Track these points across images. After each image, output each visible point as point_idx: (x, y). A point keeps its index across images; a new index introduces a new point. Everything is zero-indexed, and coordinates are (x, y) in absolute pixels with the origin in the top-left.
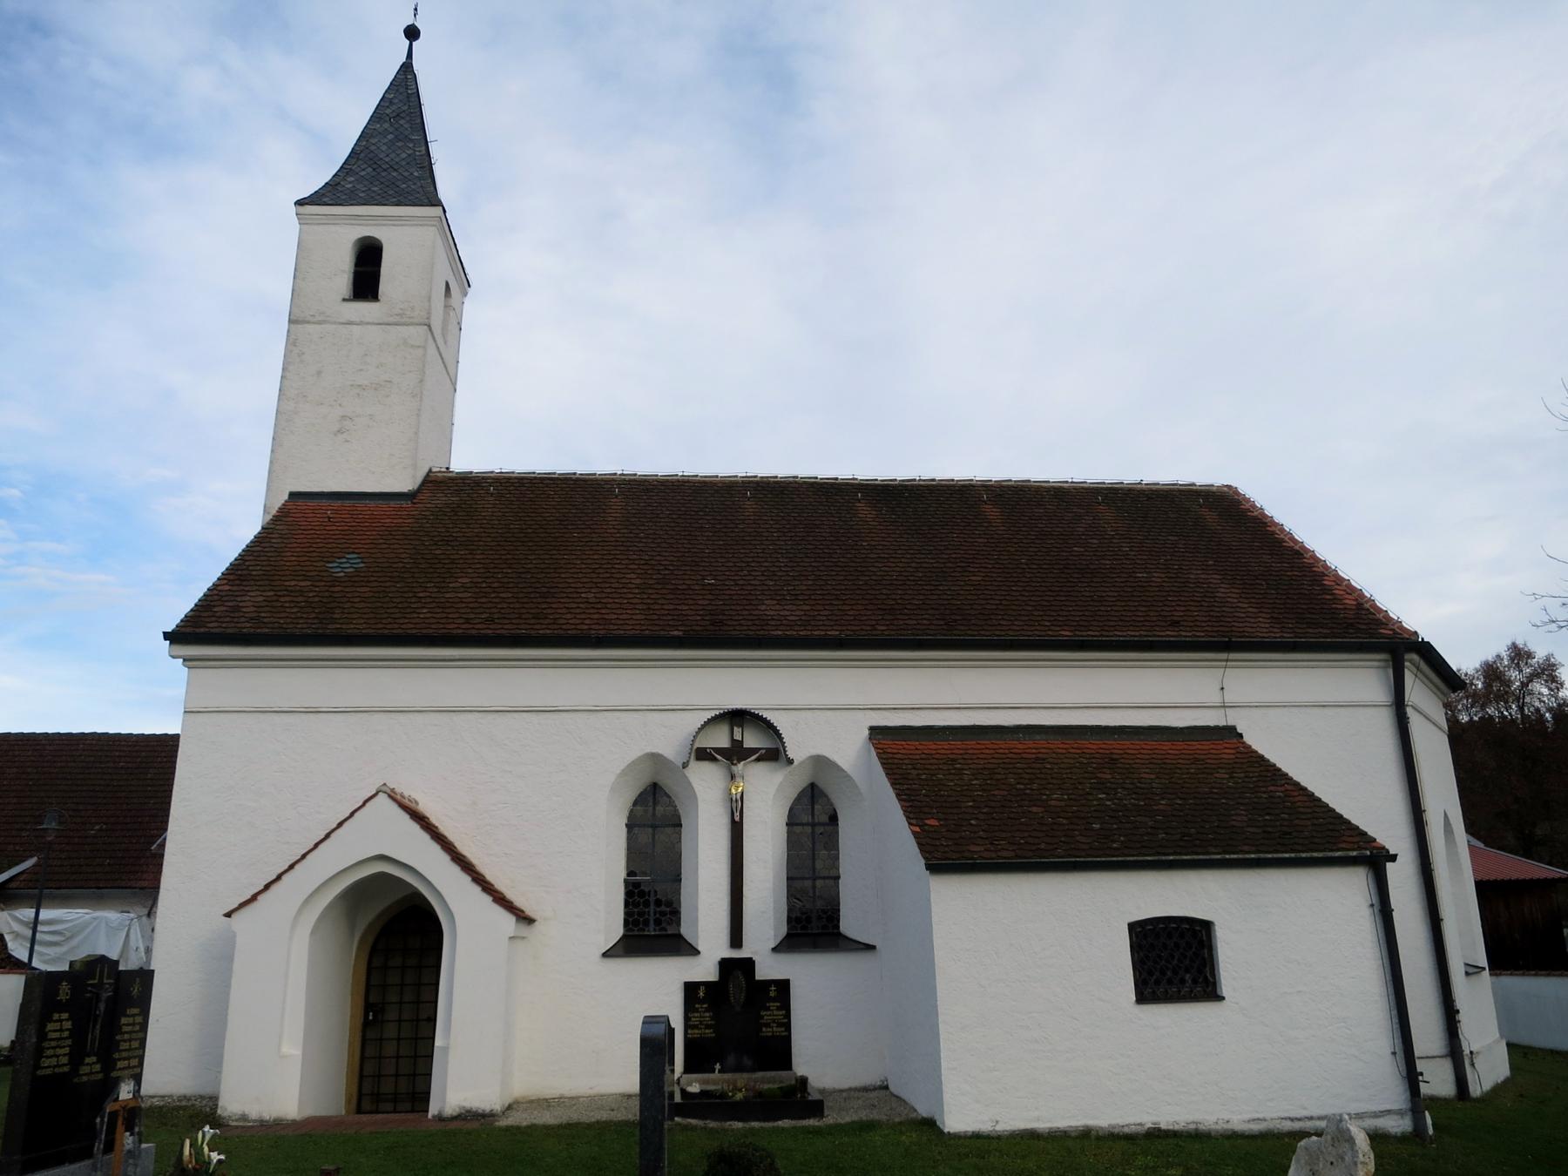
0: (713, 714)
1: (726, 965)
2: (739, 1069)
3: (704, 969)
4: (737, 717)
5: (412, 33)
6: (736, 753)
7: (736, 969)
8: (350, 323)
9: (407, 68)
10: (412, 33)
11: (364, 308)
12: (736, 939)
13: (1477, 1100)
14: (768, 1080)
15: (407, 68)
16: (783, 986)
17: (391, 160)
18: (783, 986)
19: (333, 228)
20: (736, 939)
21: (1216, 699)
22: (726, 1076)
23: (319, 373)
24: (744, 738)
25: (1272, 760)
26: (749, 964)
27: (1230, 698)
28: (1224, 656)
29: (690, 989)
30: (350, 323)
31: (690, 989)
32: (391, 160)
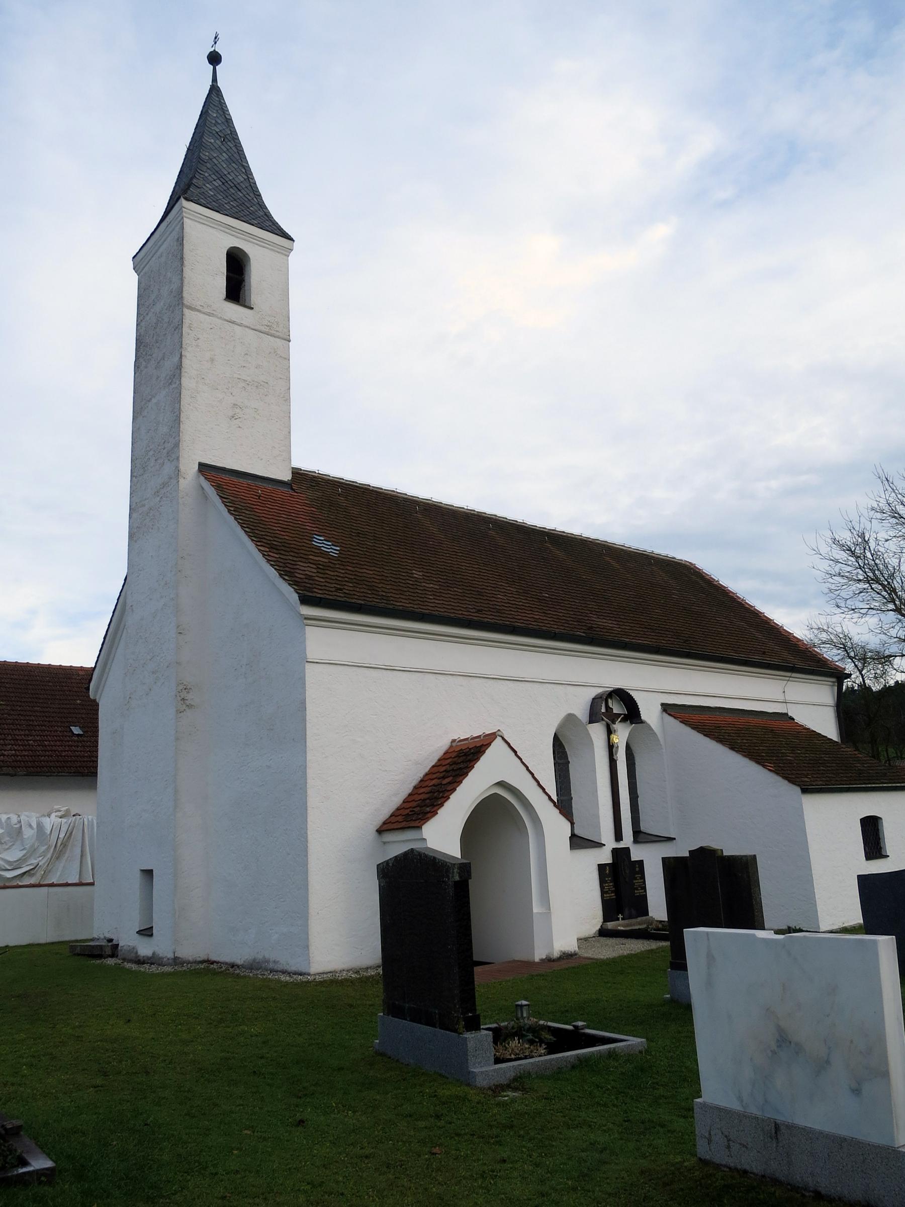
0: (600, 690)
1: (615, 852)
2: (630, 917)
3: (605, 856)
4: (622, 695)
5: (214, 59)
6: (613, 718)
7: (621, 855)
8: (233, 322)
9: (215, 91)
10: (214, 59)
11: (233, 310)
12: (618, 837)
13: (482, 1089)
14: (637, 924)
15: (215, 91)
16: (641, 863)
17: (215, 171)
18: (641, 863)
19: (211, 230)
20: (618, 837)
21: (781, 699)
22: (626, 922)
23: (212, 360)
24: (617, 707)
25: (453, 797)
26: (627, 850)
27: (788, 698)
28: (789, 674)
29: (601, 867)
30: (233, 322)
31: (601, 867)
32: (215, 171)
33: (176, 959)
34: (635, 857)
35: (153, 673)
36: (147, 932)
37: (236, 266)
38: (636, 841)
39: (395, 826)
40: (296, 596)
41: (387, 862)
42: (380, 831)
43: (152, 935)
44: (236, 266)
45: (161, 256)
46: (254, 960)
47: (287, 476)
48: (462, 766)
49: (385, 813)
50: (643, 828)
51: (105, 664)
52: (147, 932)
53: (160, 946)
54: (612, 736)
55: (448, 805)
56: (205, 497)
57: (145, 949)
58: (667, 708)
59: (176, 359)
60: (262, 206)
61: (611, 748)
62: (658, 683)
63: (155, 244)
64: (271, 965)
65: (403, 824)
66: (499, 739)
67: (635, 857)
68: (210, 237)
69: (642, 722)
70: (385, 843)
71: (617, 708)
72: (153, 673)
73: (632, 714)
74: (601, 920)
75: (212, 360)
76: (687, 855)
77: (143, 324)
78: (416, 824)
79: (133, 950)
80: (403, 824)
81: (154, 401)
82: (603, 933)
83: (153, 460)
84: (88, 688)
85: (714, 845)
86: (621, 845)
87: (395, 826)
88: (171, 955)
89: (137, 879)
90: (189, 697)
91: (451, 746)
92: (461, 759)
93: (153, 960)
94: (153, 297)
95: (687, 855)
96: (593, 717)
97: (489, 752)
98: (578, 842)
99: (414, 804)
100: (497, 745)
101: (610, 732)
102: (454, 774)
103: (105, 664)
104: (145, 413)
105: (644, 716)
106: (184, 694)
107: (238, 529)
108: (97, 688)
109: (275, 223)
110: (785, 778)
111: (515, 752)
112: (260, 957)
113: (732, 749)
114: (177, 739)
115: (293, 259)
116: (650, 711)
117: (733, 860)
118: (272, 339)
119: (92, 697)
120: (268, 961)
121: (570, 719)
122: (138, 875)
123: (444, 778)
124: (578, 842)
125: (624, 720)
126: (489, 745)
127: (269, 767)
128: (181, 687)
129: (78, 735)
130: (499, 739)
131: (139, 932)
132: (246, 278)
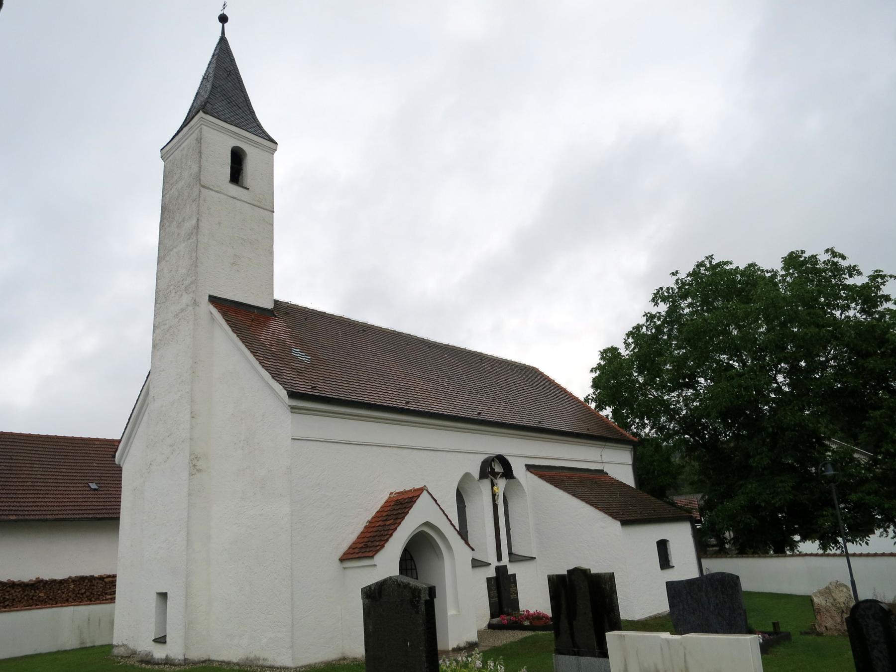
0: (487, 456)
1: (498, 569)
3: (491, 573)
4: (502, 460)
5: (223, 19)
6: (495, 474)
9: (223, 41)
10: (223, 19)
11: (234, 190)
12: (499, 558)
15: (223, 41)
17: (223, 93)
20: (499, 558)
21: (600, 460)
24: (496, 468)
27: (604, 460)
29: (489, 580)
31: (489, 580)
33: (185, 660)
34: (510, 572)
35: (171, 446)
36: (161, 640)
37: (237, 158)
38: (510, 561)
39: (351, 556)
40: (285, 392)
41: (370, 587)
42: (342, 560)
43: (165, 642)
44: (237, 158)
45: (183, 149)
46: (247, 659)
47: (270, 306)
48: (399, 511)
49: (345, 547)
50: (514, 551)
51: (129, 438)
52: (161, 640)
53: (174, 650)
54: (495, 488)
55: (391, 540)
56: (213, 319)
57: (159, 653)
58: (529, 468)
59: (194, 222)
60: (255, 120)
61: (494, 495)
62: (521, 452)
63: (178, 142)
64: (261, 663)
65: (360, 555)
66: (425, 492)
67: (510, 572)
68: (220, 139)
69: (513, 477)
70: (345, 568)
71: (498, 468)
72: (171, 446)
73: (508, 473)
74: (489, 617)
75: (219, 224)
76: (566, 573)
77: (167, 196)
78: (371, 554)
79: (149, 654)
80: (360, 555)
81: (175, 250)
82: (490, 626)
83: (173, 294)
84: (114, 457)
85: (585, 566)
86: (502, 564)
87: (351, 556)
88: (181, 657)
89: (153, 600)
90: (198, 464)
91: (390, 498)
92: (399, 506)
93: (168, 662)
94: (176, 178)
95: (566, 573)
96: (483, 475)
97: (419, 502)
98: (477, 564)
99: (366, 540)
100: (424, 497)
101: (493, 485)
102: (394, 517)
103: (129, 438)
104: (167, 259)
105: (515, 474)
106: (195, 462)
107: (240, 343)
108: (121, 459)
109: (264, 132)
110: (611, 515)
111: (436, 501)
112: (252, 656)
113: (574, 495)
114: (189, 495)
115: (276, 153)
116: (519, 470)
117: (598, 577)
118: (261, 210)
119: (117, 462)
120: (258, 659)
121: (467, 476)
122: (155, 596)
123: (386, 520)
124: (477, 564)
125: (502, 477)
126: (418, 496)
127: (261, 515)
128: (193, 456)
129: (95, 490)
130: (425, 492)
131: (155, 641)
132: (244, 168)
